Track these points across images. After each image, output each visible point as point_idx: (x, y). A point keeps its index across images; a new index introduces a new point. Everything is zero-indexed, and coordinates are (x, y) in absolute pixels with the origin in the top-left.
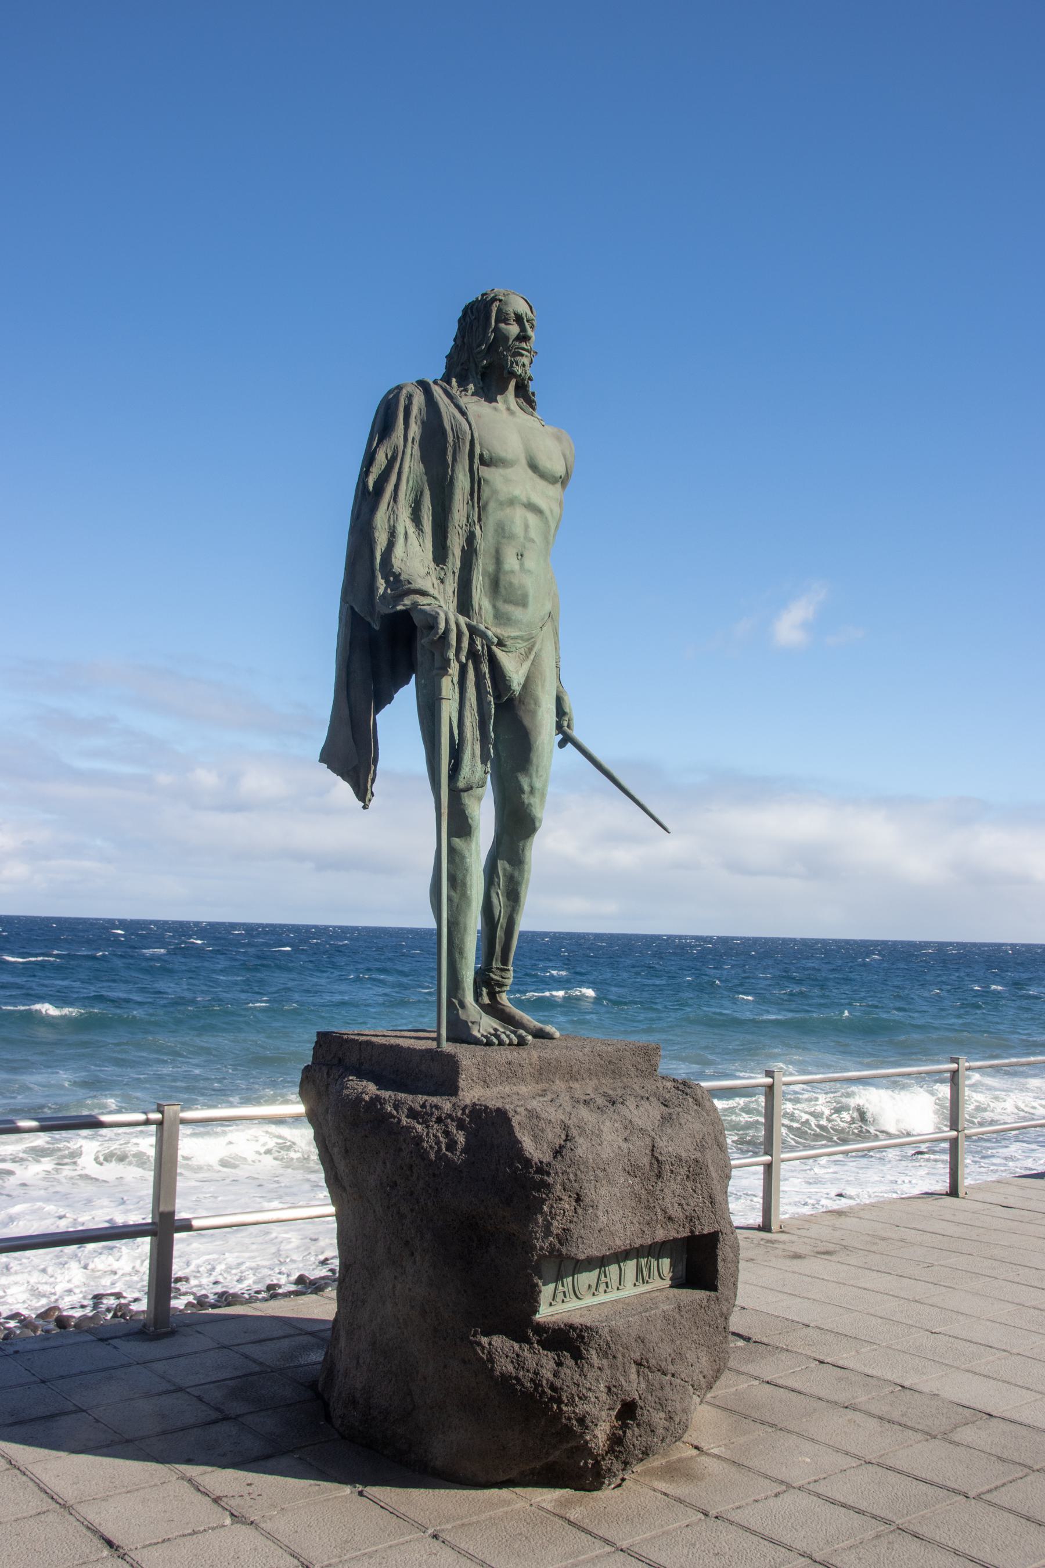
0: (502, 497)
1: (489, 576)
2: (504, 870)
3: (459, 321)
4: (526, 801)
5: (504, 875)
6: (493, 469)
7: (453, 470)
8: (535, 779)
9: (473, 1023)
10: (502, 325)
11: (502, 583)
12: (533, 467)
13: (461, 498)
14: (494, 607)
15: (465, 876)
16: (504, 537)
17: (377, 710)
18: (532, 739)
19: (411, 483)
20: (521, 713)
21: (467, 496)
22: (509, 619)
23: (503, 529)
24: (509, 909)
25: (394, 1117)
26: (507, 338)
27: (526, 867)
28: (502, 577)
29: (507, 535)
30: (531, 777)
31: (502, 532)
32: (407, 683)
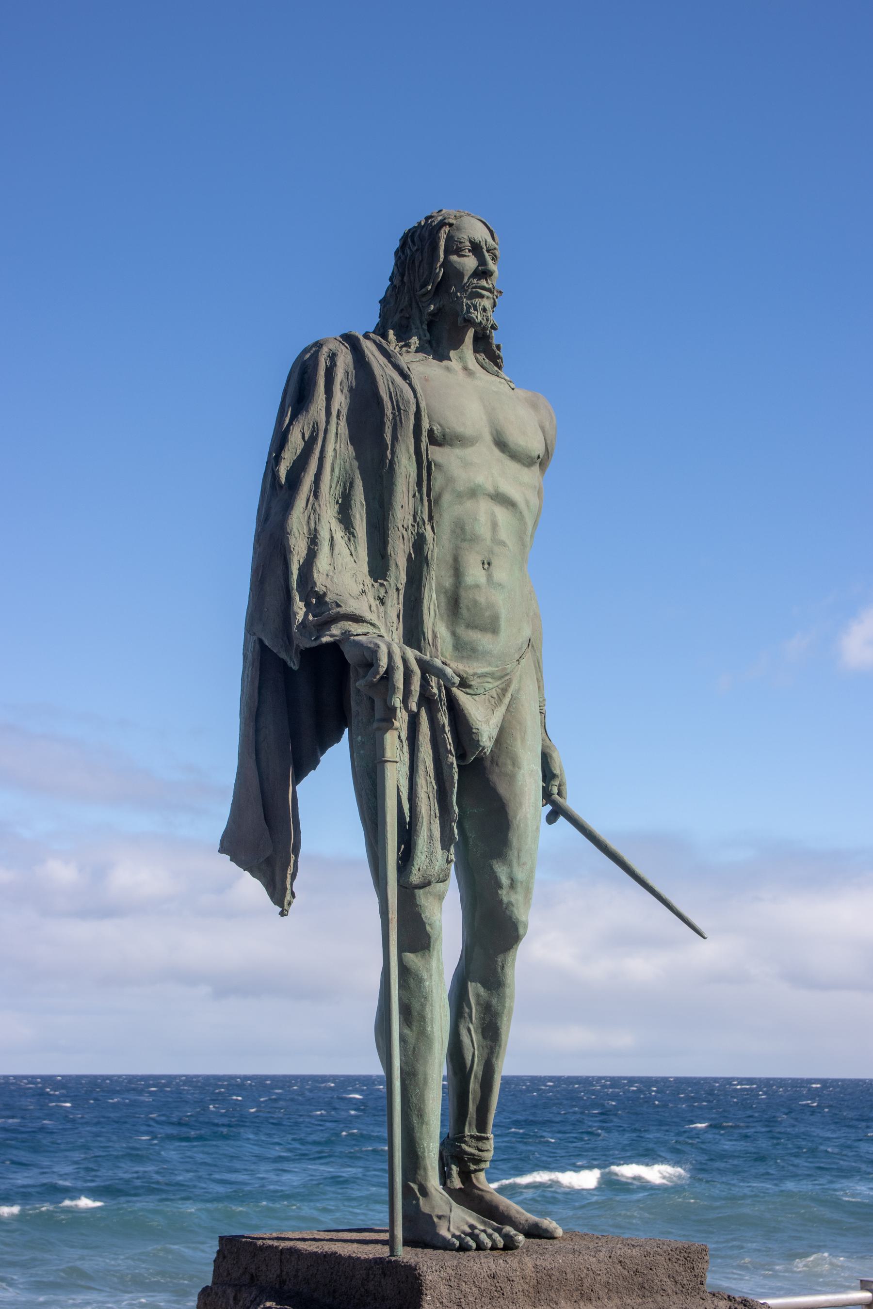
0: (461, 486)
1: (446, 592)
2: (478, 995)
3: (396, 253)
4: (505, 899)
5: (478, 1003)
6: (446, 450)
7: (393, 453)
8: (516, 868)
9: (440, 1217)
10: (454, 258)
11: (464, 602)
12: (501, 444)
13: (405, 489)
14: (454, 634)
15: (423, 1006)
16: (464, 540)
17: (299, 776)
18: (511, 814)
19: (337, 471)
20: (494, 778)
21: (413, 487)
22: (474, 650)
23: (462, 529)
24: (486, 1051)
26: (460, 274)
27: (508, 991)
28: (463, 594)
29: (468, 537)
30: (510, 866)
31: (462, 533)
32: (338, 740)
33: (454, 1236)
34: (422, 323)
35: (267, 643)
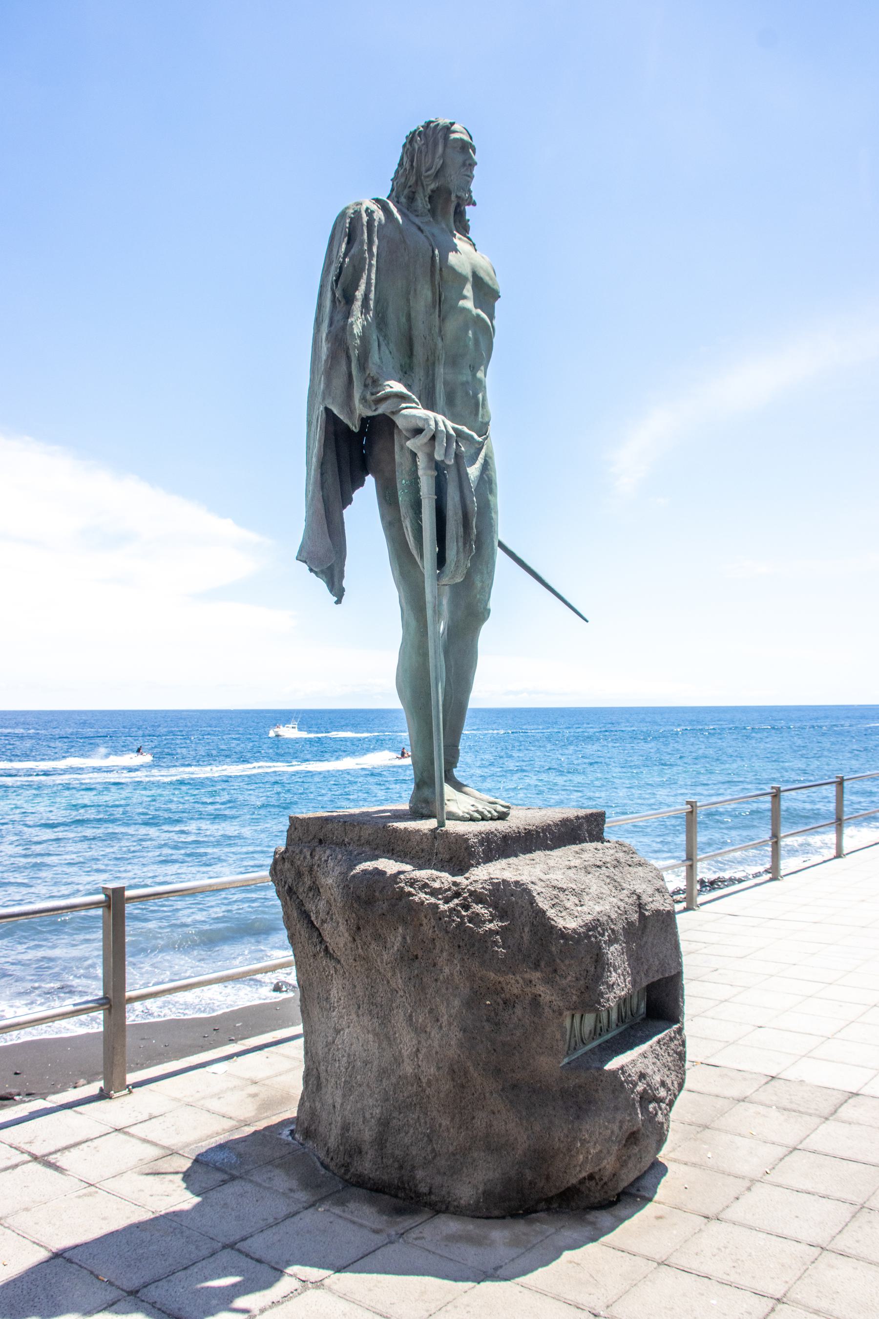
25: (413, 895)
33: (464, 812)
34: (425, 196)
35: (336, 412)
